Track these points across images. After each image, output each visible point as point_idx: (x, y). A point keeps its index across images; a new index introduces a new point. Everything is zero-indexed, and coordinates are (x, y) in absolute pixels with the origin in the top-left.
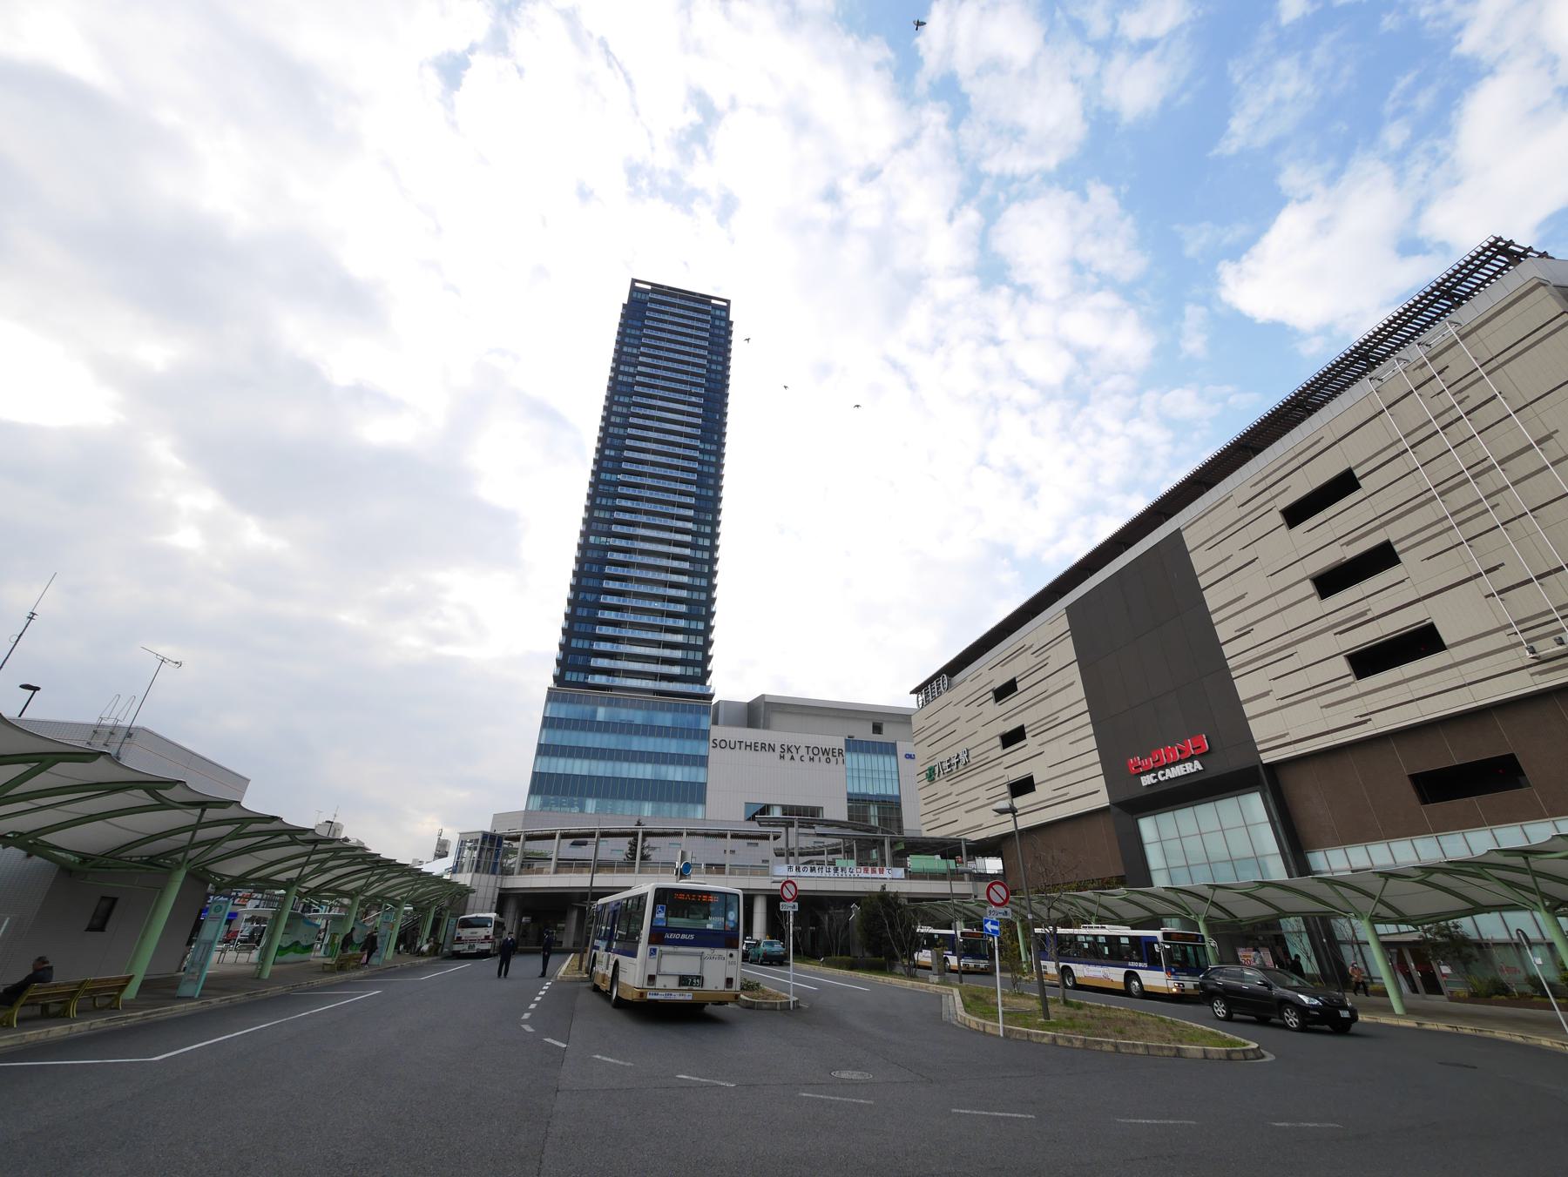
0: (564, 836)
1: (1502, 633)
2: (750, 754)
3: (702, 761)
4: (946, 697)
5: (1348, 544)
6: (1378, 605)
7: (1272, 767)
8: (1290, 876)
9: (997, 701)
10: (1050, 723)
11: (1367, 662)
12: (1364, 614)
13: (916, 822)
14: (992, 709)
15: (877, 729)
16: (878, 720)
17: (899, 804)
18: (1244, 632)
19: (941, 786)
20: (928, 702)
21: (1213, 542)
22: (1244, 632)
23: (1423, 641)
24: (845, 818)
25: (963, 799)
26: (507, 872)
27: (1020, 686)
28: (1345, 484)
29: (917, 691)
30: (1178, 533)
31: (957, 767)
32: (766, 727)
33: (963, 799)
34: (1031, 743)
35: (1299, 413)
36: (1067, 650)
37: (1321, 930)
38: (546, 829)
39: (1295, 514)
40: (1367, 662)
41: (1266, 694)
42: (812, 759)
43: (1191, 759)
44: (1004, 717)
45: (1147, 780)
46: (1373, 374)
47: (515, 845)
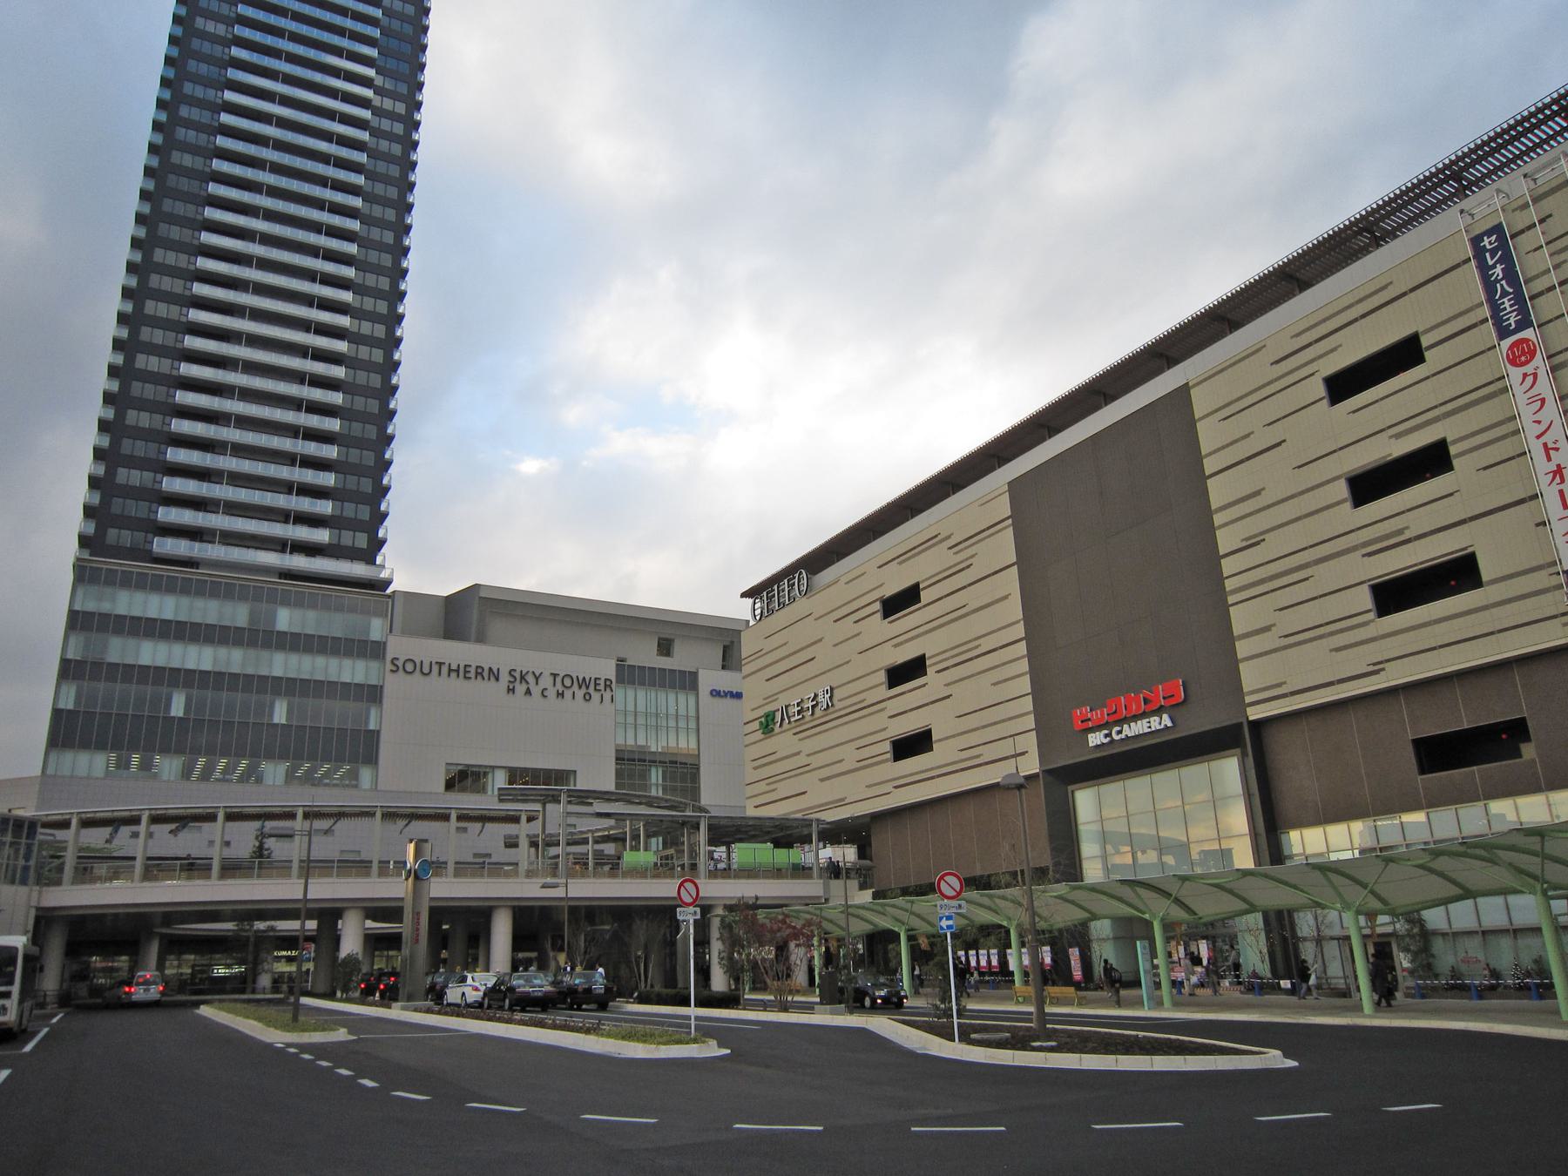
0: (156, 819)
1: (1544, 573)
2: (456, 683)
3: (373, 694)
4: (802, 606)
5: (1398, 436)
6: (1419, 522)
7: (1257, 726)
8: (1258, 862)
9: (886, 616)
10: (965, 655)
11: (1394, 595)
12: (1400, 532)
13: (718, 795)
14: (878, 627)
15: (665, 648)
16: (667, 633)
17: (697, 767)
18: (1252, 543)
19: (784, 741)
20: (771, 611)
21: (1229, 410)
22: (1252, 543)
23: (1458, 574)
24: (610, 785)
25: (816, 761)
26: (51, 877)
27: (925, 596)
28: (1406, 354)
29: (751, 593)
30: (1184, 390)
31: (815, 714)
32: (481, 639)
33: (816, 761)
34: (932, 680)
35: (1364, 239)
36: (1004, 547)
37: (1280, 925)
38: (121, 808)
39: (1342, 386)
40: (1394, 595)
41: (1267, 629)
42: (560, 695)
43: (1158, 711)
44: (898, 640)
45: (1096, 739)
46: (1465, 204)
47: (60, 834)
